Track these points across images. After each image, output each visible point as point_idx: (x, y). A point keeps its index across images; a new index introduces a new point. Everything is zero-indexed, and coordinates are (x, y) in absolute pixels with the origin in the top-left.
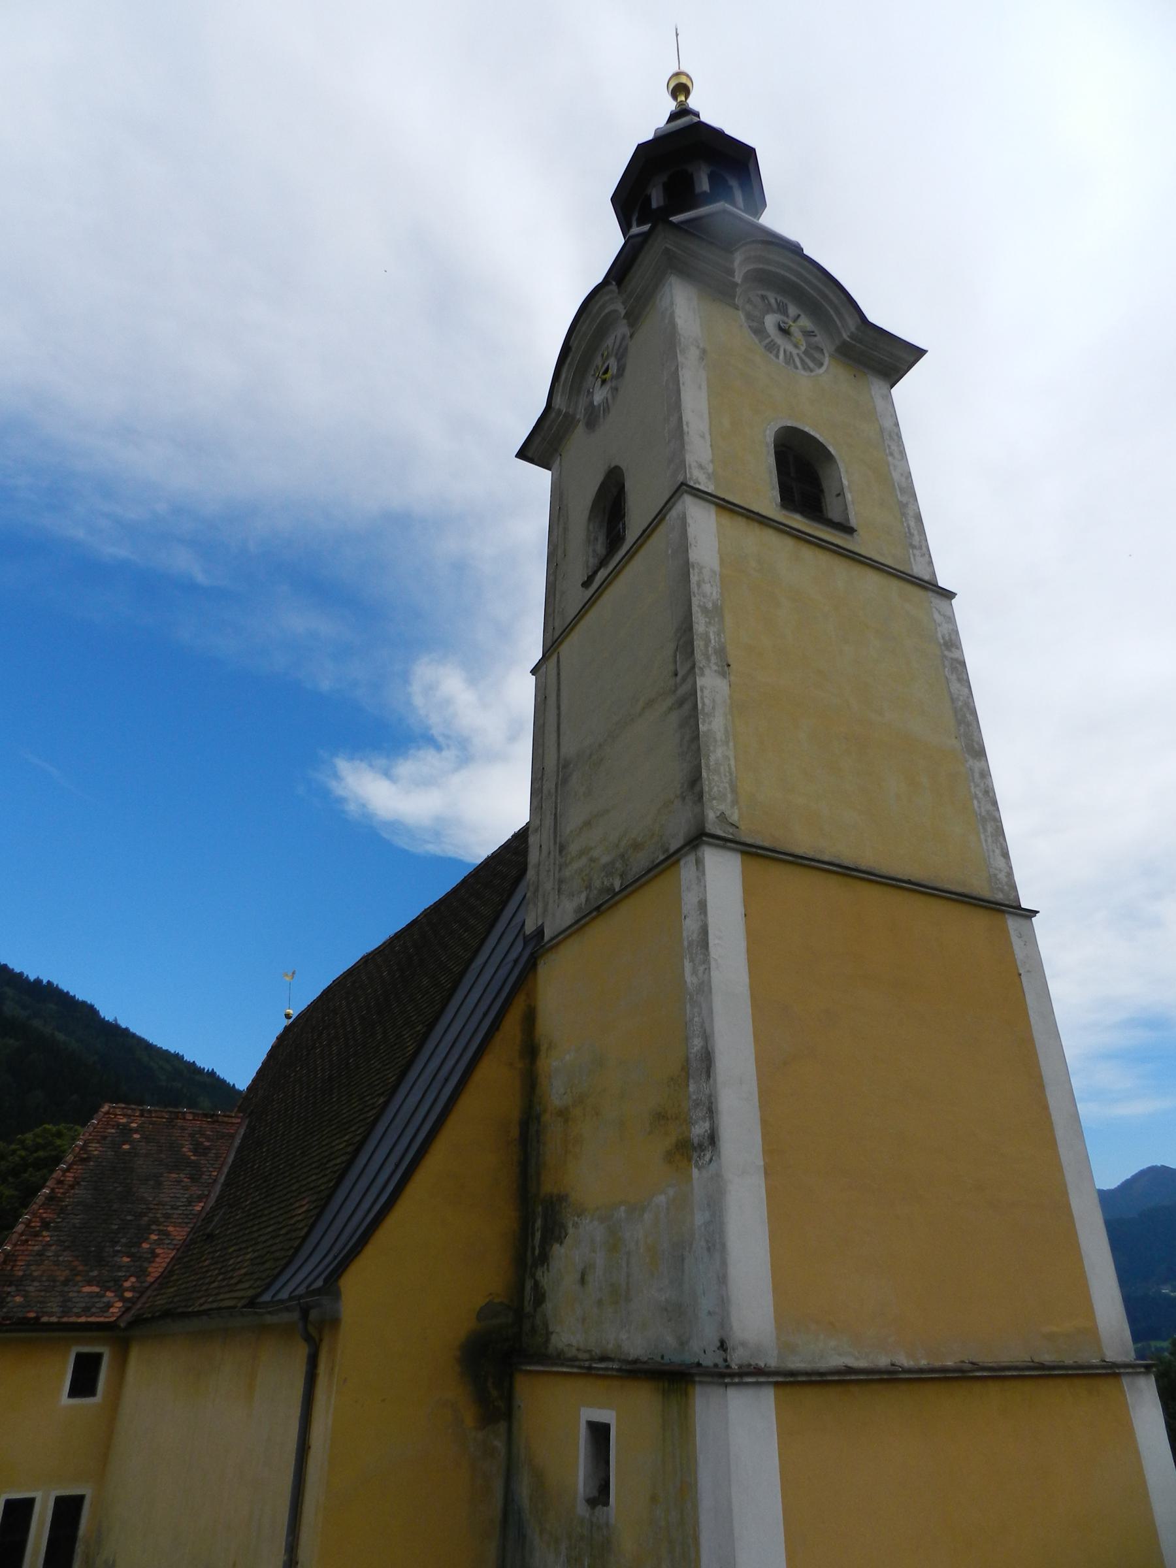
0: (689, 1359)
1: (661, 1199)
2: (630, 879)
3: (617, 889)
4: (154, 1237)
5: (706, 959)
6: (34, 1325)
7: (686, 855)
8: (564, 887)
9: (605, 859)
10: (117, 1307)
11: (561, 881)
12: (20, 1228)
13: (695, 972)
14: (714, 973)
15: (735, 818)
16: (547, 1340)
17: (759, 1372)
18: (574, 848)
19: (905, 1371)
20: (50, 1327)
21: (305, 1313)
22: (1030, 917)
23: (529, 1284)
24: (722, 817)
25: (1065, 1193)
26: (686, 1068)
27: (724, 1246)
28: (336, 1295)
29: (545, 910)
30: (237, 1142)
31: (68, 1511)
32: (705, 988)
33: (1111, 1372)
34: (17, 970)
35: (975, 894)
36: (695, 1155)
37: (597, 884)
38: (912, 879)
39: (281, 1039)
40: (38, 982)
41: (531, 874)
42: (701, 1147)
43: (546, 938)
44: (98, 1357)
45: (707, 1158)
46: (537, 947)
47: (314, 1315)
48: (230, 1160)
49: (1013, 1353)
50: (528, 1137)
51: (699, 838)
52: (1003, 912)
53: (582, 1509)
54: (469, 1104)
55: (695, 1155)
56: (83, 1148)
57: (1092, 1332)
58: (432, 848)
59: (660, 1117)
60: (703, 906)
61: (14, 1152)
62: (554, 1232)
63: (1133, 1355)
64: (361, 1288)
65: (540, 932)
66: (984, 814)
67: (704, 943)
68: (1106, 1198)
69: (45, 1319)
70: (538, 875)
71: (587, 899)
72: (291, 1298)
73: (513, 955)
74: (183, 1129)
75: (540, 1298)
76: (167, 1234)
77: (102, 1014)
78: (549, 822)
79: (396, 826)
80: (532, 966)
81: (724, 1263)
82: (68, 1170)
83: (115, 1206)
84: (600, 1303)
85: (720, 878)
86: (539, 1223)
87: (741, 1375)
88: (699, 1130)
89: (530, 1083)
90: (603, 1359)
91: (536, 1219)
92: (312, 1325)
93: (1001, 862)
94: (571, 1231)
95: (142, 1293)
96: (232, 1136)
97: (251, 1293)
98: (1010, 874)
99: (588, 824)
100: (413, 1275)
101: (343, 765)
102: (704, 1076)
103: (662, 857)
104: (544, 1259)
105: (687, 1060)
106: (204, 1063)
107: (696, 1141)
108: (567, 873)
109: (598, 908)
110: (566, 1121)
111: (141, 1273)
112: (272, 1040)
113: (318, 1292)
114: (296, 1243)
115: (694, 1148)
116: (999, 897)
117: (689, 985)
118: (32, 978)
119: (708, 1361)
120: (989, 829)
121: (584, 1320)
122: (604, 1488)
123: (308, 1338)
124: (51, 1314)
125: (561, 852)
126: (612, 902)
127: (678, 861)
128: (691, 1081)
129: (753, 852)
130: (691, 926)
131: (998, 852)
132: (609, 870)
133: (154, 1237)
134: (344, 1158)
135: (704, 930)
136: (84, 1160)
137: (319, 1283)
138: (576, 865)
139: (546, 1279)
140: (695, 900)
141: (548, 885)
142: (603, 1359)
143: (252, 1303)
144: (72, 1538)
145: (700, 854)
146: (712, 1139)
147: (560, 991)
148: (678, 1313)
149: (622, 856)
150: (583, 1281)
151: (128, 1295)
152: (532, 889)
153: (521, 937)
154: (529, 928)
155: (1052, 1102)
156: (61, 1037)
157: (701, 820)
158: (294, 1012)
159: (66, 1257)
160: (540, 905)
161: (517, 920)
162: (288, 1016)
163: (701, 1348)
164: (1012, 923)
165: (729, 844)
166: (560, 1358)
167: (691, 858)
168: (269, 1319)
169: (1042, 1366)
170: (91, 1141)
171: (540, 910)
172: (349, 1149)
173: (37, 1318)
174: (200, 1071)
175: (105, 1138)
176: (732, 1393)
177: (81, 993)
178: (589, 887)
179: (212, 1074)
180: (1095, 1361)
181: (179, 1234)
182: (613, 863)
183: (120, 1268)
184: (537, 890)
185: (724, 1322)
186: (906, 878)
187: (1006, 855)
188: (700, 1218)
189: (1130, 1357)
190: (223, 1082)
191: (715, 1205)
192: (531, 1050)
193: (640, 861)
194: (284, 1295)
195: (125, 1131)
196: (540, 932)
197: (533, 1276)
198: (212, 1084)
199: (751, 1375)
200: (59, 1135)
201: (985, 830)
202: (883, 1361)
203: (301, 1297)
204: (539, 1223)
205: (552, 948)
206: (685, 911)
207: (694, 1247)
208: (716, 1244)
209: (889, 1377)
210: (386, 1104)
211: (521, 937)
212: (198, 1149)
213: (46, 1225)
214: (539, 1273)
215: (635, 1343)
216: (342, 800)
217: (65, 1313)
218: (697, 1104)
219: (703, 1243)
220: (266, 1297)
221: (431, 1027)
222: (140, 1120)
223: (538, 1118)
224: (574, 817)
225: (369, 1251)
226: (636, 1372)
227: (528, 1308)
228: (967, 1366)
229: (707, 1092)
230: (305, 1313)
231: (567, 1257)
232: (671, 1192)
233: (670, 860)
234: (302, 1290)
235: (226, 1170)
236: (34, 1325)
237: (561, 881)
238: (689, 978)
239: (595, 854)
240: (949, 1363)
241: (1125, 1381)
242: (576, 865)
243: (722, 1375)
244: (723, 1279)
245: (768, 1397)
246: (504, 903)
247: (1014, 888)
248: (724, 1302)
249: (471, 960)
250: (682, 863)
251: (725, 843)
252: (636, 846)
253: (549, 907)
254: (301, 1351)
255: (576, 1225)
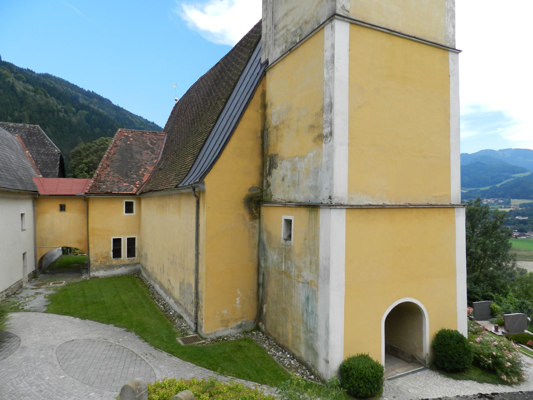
0: (318, 202)
1: (311, 154)
2: (303, 37)
3: (298, 41)
4: (143, 170)
5: (333, 68)
6: (110, 194)
7: (327, 24)
8: (276, 43)
9: (293, 29)
10: (135, 189)
11: (275, 40)
12: (100, 166)
13: (328, 73)
14: (336, 73)
15: (348, 8)
16: (271, 197)
17: (342, 205)
18: (280, 26)
19: (388, 206)
20: (115, 194)
21: (194, 189)
22: (458, 53)
23: (265, 182)
24: (343, 7)
25: (450, 154)
26: (322, 110)
27: (333, 168)
28: (204, 184)
29: (269, 53)
30: (165, 142)
31: (131, 242)
32: (332, 79)
33: (453, 207)
34: (81, 87)
35: (439, 43)
36: (324, 139)
37: (290, 40)
38: (416, 36)
39: (175, 108)
40: (89, 91)
41: (263, 38)
42: (327, 136)
43: (269, 64)
44: (132, 203)
45: (329, 140)
46: (266, 67)
47: (196, 189)
48: (163, 147)
49: (424, 202)
50: (264, 135)
51: (333, 16)
52: (448, 51)
53: (283, 241)
54: (243, 124)
55: (324, 139)
56: (115, 142)
57: (449, 196)
58: (221, 42)
59: (312, 127)
60: (333, 46)
61: (94, 146)
62: (273, 166)
63: (460, 202)
64: (211, 181)
65: (267, 62)
66: (449, 8)
67: (333, 61)
68: (464, 157)
69: (113, 192)
70: (266, 39)
71: (286, 47)
72: (189, 185)
73: (257, 71)
74: (146, 137)
75: (269, 185)
76: (147, 169)
77: (113, 103)
78: (270, 15)
79: (207, 32)
80: (264, 74)
81: (332, 173)
82: (111, 149)
83: (129, 160)
84: (289, 186)
85: (341, 31)
86: (268, 163)
87: (336, 206)
88: (326, 131)
89: (264, 117)
90: (290, 202)
91: (267, 162)
92: (197, 192)
93: (451, 30)
94: (279, 165)
95: (142, 186)
96: (163, 139)
97: (176, 184)
98: (454, 35)
99: (286, 15)
100: (229, 176)
101: (185, 7)
102: (329, 112)
103: (317, 27)
104: (270, 174)
105: (323, 106)
106: (150, 120)
107: (325, 134)
108: (277, 37)
109: (290, 50)
110: (278, 130)
111: (141, 180)
112: (172, 109)
113: (197, 182)
114: (188, 170)
115: (322, 136)
116: (448, 45)
117: (325, 77)
118: (87, 90)
119: (325, 202)
120: (450, 15)
121: (283, 191)
122: (290, 237)
123: (196, 196)
124: (115, 191)
125: (275, 28)
126: (295, 47)
127: (324, 27)
128: (324, 114)
129: (355, 22)
130: (327, 55)
131: (451, 25)
132: (294, 34)
133: (143, 170)
134: (201, 144)
135: (333, 56)
136: (115, 146)
137: (198, 180)
138: (281, 33)
139: (270, 180)
140: (330, 44)
141: (270, 43)
142: (290, 202)
143: (176, 187)
144: (134, 249)
145: (333, 23)
146: (331, 134)
147: (275, 85)
148: (315, 188)
149: (300, 28)
150: (283, 180)
151: (138, 186)
152: (263, 45)
153: (260, 64)
154: (263, 61)
155: (452, 123)
156: (101, 110)
157: (335, 10)
158: (178, 99)
159: (116, 175)
160: (267, 51)
161: (258, 58)
162: (176, 100)
163: (323, 198)
164: (451, 55)
165: (345, 19)
166: (275, 202)
167: (329, 26)
168: (183, 191)
169: (431, 205)
170: (117, 140)
171: (267, 53)
172: (203, 141)
173: (111, 192)
174: (149, 122)
175: (121, 139)
176: (332, 210)
177: (105, 95)
178: (286, 42)
179: (153, 123)
180: (448, 204)
181: (151, 169)
182: (296, 31)
183: (134, 178)
184: (265, 44)
185: (331, 191)
186: (413, 35)
187: (454, 27)
188: (324, 160)
189: (459, 203)
190: (157, 126)
191: (330, 156)
192: (264, 106)
193: (308, 29)
194: (187, 184)
195: (127, 137)
196: (267, 62)
197: (266, 179)
198: (153, 127)
199: (340, 206)
200: (107, 141)
201: (448, 16)
202: (381, 203)
203: (192, 184)
204: (268, 163)
205: (272, 67)
206: (325, 49)
207: (321, 169)
208: (330, 168)
209: (382, 207)
210: (214, 126)
211: (260, 64)
212: (152, 143)
213: (108, 166)
214: (268, 178)
215: (301, 198)
216: (186, 22)
217: (120, 191)
218: (326, 122)
219: (326, 168)
220: (181, 185)
221: (227, 99)
222: (132, 134)
223: (267, 130)
224: (279, 14)
225: (212, 171)
226: (300, 205)
227: (265, 188)
228: (407, 205)
229: (330, 118)
230: (194, 189)
231: (277, 174)
232: (315, 152)
233: (321, 27)
234: (192, 182)
235: (162, 150)
236: (110, 194)
237: (275, 40)
238: (326, 76)
239: (289, 27)
240: (402, 204)
241: (456, 209)
242: (281, 33)
243: (330, 206)
244: (331, 178)
245: (344, 212)
246: (252, 53)
247: (454, 41)
248: (331, 185)
249: (241, 75)
250: (325, 28)
251: (344, 18)
252: (306, 23)
253: (269, 51)
254: (194, 200)
255: (281, 163)
